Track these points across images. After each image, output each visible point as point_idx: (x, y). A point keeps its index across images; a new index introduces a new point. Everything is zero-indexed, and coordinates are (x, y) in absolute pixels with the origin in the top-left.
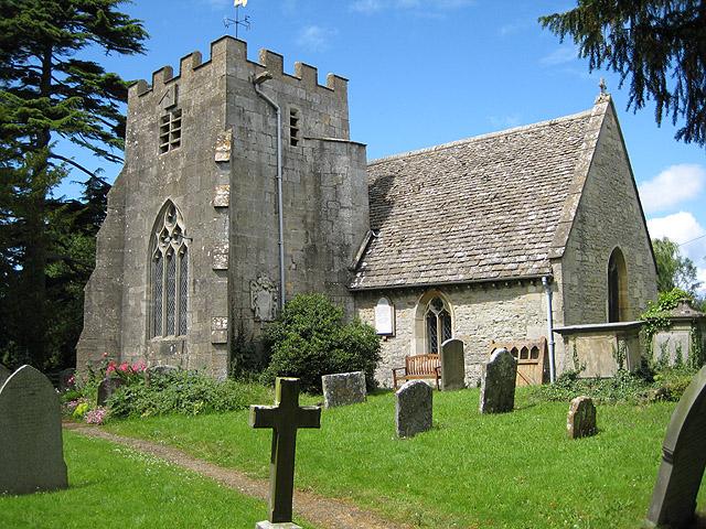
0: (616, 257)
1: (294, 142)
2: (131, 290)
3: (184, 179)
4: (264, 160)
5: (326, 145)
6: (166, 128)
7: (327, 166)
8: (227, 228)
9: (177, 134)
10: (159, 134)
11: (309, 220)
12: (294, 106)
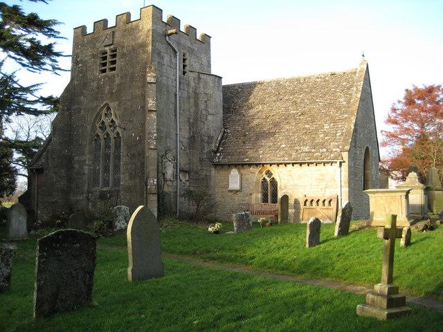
0: (367, 149)
1: (184, 73)
2: (76, 158)
3: (119, 91)
4: (170, 83)
5: (202, 76)
6: (105, 58)
7: (202, 89)
8: (155, 123)
9: (114, 62)
10: (99, 61)
11: (191, 121)
12: (185, 51)
